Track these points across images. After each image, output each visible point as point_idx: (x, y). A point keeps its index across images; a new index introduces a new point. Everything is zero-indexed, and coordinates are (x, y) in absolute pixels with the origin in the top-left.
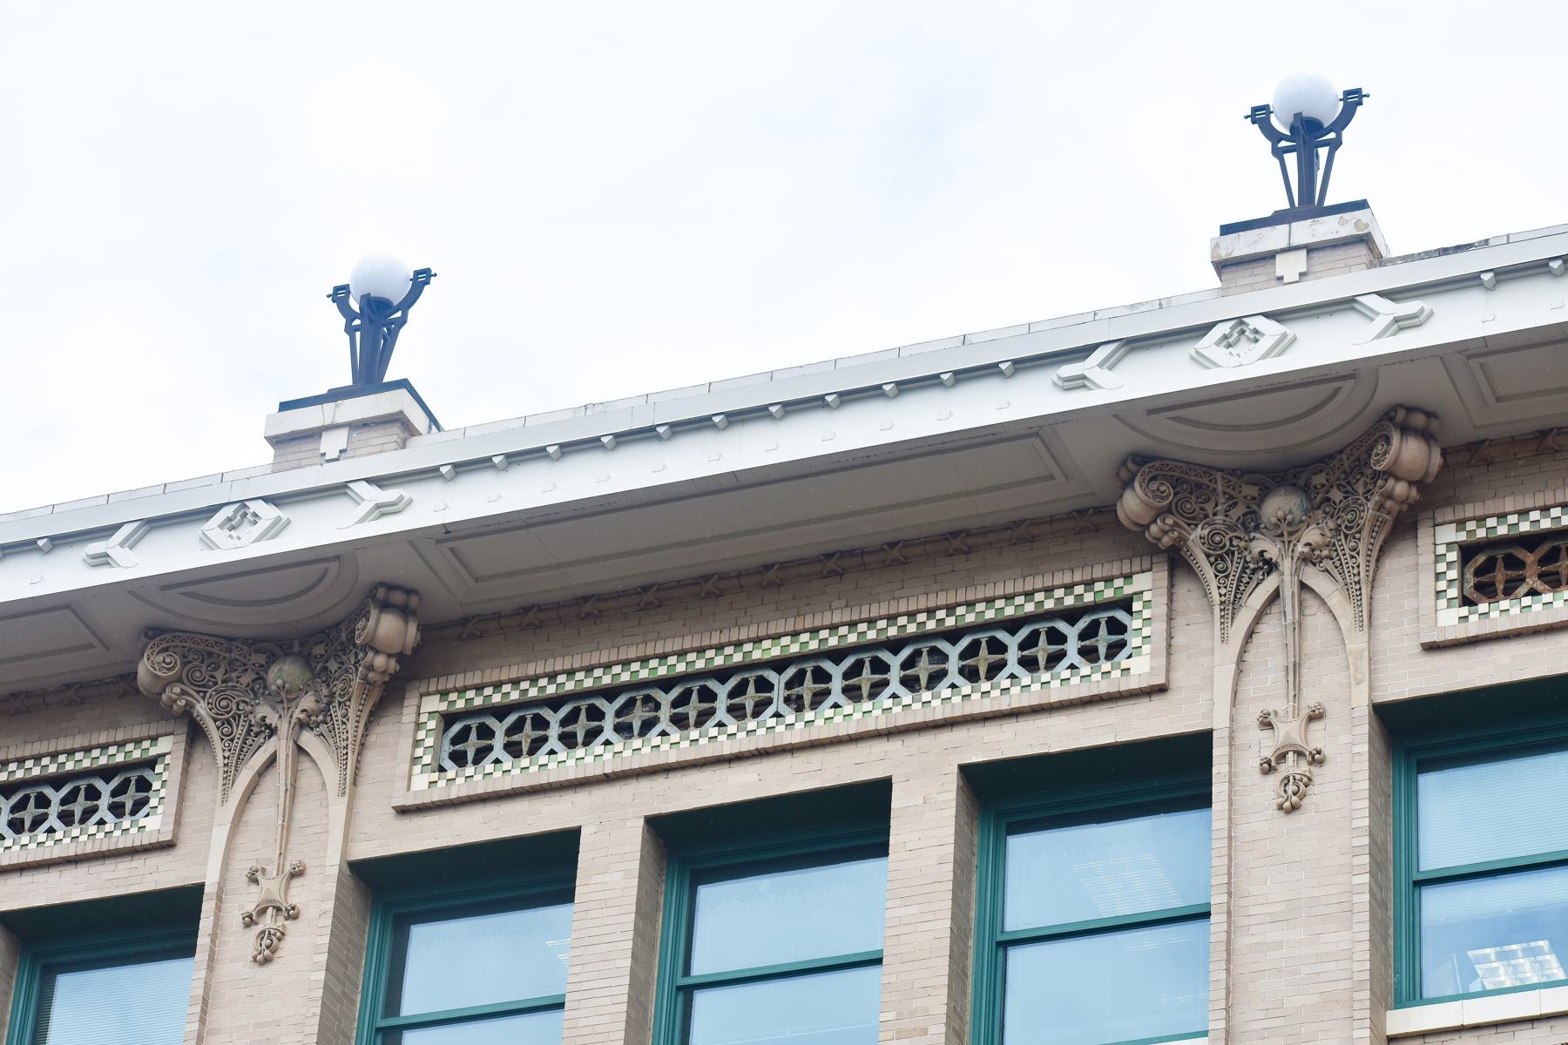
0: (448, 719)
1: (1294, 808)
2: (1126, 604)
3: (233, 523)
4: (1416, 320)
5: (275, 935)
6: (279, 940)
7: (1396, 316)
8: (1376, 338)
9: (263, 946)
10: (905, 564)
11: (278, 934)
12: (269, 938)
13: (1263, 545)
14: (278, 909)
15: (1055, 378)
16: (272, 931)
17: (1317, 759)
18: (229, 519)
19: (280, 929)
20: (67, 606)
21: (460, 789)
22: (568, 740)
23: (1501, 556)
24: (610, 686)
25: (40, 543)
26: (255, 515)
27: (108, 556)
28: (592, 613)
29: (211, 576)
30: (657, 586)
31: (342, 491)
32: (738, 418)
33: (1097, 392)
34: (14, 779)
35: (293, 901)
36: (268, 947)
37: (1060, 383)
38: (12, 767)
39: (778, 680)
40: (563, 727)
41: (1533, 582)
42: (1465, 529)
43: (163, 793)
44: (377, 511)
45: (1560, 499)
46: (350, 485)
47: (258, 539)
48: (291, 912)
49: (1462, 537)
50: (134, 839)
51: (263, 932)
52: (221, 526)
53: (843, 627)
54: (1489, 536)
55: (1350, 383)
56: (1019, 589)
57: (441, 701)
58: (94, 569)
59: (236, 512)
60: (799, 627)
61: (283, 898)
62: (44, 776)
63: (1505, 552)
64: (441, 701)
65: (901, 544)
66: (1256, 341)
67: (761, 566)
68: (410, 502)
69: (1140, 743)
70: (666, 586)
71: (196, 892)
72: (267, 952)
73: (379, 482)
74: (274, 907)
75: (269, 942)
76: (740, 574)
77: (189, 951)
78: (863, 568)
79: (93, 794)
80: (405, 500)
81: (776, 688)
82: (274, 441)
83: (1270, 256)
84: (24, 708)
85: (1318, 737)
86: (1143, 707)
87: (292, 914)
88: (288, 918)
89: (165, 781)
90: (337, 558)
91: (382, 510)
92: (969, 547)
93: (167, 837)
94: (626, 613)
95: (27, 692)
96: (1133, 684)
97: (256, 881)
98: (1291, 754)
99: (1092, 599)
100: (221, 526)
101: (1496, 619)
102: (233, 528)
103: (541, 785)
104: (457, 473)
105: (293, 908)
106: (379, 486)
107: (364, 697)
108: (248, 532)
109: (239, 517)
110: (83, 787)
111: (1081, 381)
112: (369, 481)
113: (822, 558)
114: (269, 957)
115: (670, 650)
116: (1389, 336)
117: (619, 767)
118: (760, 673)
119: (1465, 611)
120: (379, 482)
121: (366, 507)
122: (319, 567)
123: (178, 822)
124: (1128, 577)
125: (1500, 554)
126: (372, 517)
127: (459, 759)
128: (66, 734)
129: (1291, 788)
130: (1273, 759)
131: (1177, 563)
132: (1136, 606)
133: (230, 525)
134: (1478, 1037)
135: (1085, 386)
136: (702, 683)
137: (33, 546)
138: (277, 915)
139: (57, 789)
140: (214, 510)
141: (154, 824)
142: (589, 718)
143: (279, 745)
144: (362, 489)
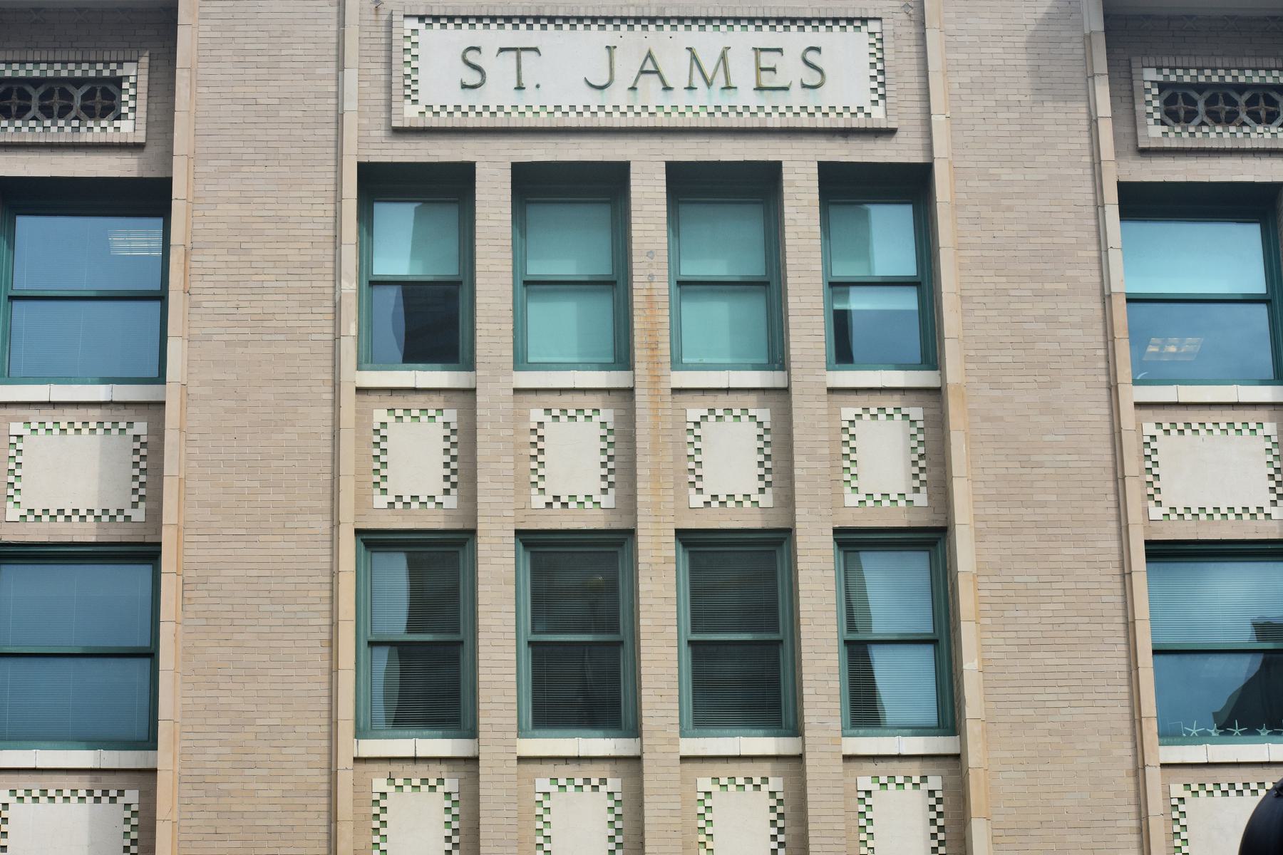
2: (118, 81)
40: (1248, 107)
41: (1244, 116)
42: (80, 69)
45: (1279, 65)
49: (1160, 78)
56: (44, 58)
57: (1157, 73)
64: (1157, 73)
67: (1225, 16)
76: (1170, 19)
94: (1173, 31)
101: (25, 133)
113: (1268, 19)
117: (16, 139)
119: (1165, 129)
124: (120, 64)
125: (15, 87)
132: (125, 85)
134: (136, 410)
141: (128, 129)
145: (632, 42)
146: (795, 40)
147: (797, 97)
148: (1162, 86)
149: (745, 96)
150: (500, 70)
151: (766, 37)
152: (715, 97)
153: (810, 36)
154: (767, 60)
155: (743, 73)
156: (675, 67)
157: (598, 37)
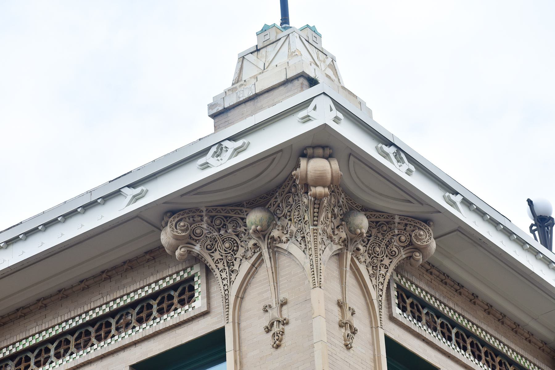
1: (278, 346)
2: (192, 278)
3: (218, 153)
4: (141, 195)
5: (279, 333)
6: (282, 335)
7: (235, 148)
8: (228, 160)
9: (275, 340)
10: (88, 288)
11: (281, 333)
12: (277, 336)
14: (279, 322)
15: (197, 166)
16: (278, 332)
18: (215, 152)
19: (281, 330)
20: (137, 216)
22: (99, 339)
23: (125, 314)
24: (166, 287)
25: (40, 228)
26: (226, 148)
27: (309, 116)
28: (22, 315)
29: (237, 169)
30: (85, 280)
31: (119, 193)
32: (10, 242)
33: (315, 121)
34: (65, 330)
35: (285, 316)
36: (277, 340)
37: (300, 120)
38: (4, 350)
39: (175, 294)
43: (199, 290)
44: (236, 152)
46: (121, 190)
47: (230, 158)
48: (285, 321)
50: (192, 313)
51: (274, 333)
52: (213, 156)
53: (64, 323)
54: (111, 310)
55: (280, 154)
58: (304, 124)
59: (217, 148)
60: (27, 335)
61: (280, 317)
62: (154, 292)
63: (188, 284)
65: (85, 281)
66: (227, 151)
68: (249, 143)
69: (199, 338)
70: (89, 279)
71: (222, 331)
72: (277, 342)
73: (233, 139)
74: (277, 321)
75: (277, 337)
77: (223, 359)
78: (11, 321)
79: (68, 342)
80: (145, 191)
81: (71, 342)
82: (213, 116)
84: (107, 277)
87: (285, 323)
88: (283, 324)
89: (200, 286)
90: (281, 151)
91: (237, 150)
92: (45, 305)
93: (205, 309)
95: (129, 260)
96: (197, 312)
97: (267, 311)
98: (275, 322)
99: (158, 289)
100: (213, 156)
102: (218, 156)
103: (150, 335)
104: (105, 201)
105: (285, 320)
106: (234, 141)
107: (316, 210)
108: (226, 155)
109: (219, 150)
110: (166, 296)
111: (308, 118)
112: (129, 186)
114: (278, 344)
115: (35, 332)
116: (234, 157)
118: (86, 329)
120: (233, 139)
121: (129, 198)
122: (272, 158)
123: (209, 304)
126: (132, 202)
128: (124, 286)
129: (276, 337)
130: (269, 326)
133: (217, 155)
135: (310, 119)
136: (188, 284)
137: (18, 239)
138: (279, 324)
139: (33, 353)
140: (208, 149)
141: (199, 304)
142: (106, 327)
144: (126, 191)
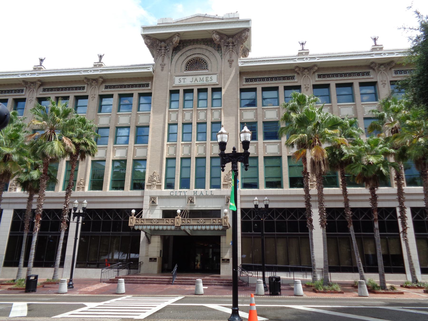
0: (105, 86)
2: (294, 76)
13: (31, 87)
17: (309, 88)
21: (247, 84)
83: (302, 53)
85: (309, 86)
86: (296, 83)
87: (95, 98)
127: (247, 82)
131: (298, 74)
143: (32, 89)
145: (194, 77)
146: (210, 76)
147: (210, 82)
148: (245, 79)
149: (205, 82)
150: (182, 81)
151: (207, 76)
152: (201, 82)
153: (211, 76)
154: (207, 78)
155: (205, 79)
156: (198, 80)
157: (191, 77)
